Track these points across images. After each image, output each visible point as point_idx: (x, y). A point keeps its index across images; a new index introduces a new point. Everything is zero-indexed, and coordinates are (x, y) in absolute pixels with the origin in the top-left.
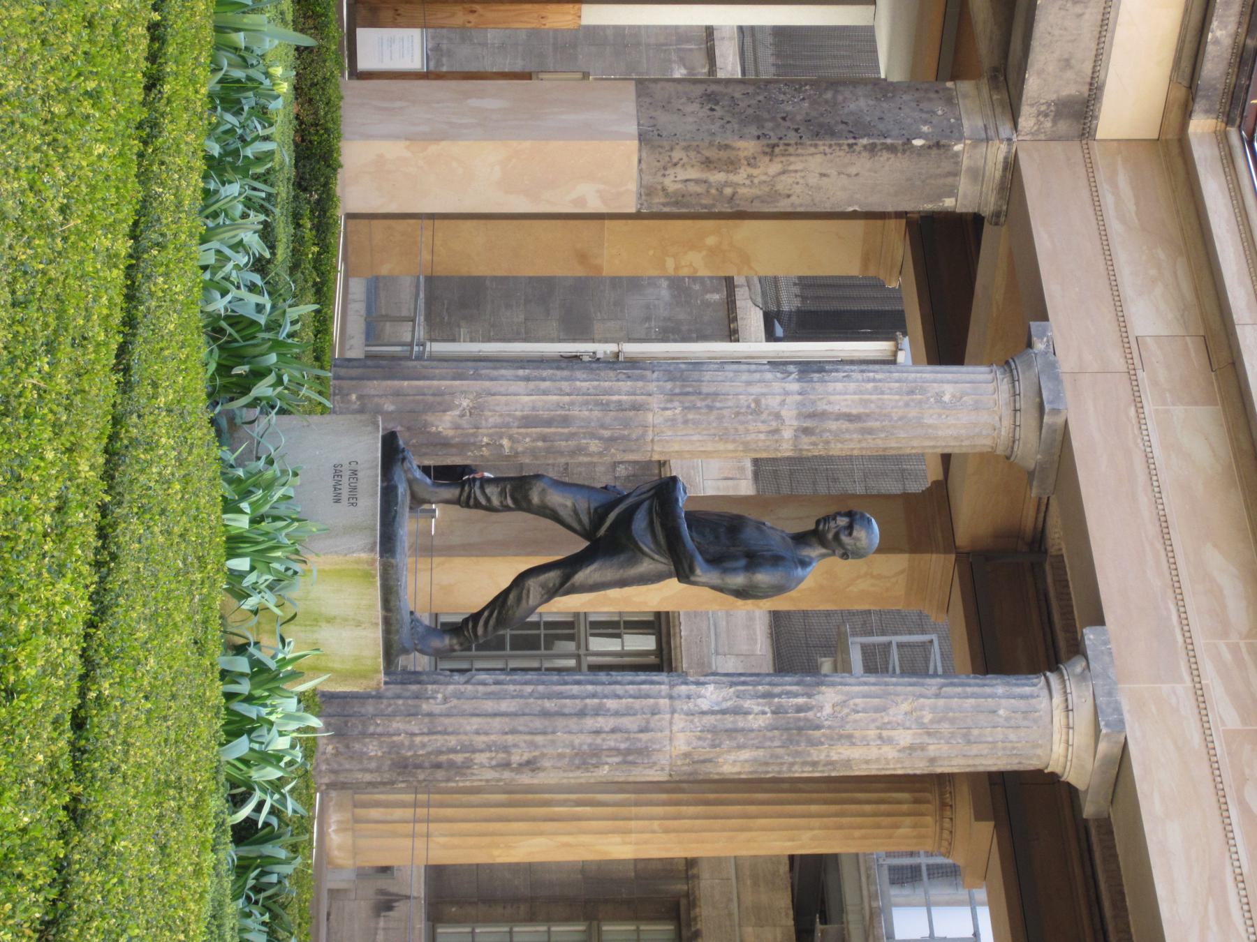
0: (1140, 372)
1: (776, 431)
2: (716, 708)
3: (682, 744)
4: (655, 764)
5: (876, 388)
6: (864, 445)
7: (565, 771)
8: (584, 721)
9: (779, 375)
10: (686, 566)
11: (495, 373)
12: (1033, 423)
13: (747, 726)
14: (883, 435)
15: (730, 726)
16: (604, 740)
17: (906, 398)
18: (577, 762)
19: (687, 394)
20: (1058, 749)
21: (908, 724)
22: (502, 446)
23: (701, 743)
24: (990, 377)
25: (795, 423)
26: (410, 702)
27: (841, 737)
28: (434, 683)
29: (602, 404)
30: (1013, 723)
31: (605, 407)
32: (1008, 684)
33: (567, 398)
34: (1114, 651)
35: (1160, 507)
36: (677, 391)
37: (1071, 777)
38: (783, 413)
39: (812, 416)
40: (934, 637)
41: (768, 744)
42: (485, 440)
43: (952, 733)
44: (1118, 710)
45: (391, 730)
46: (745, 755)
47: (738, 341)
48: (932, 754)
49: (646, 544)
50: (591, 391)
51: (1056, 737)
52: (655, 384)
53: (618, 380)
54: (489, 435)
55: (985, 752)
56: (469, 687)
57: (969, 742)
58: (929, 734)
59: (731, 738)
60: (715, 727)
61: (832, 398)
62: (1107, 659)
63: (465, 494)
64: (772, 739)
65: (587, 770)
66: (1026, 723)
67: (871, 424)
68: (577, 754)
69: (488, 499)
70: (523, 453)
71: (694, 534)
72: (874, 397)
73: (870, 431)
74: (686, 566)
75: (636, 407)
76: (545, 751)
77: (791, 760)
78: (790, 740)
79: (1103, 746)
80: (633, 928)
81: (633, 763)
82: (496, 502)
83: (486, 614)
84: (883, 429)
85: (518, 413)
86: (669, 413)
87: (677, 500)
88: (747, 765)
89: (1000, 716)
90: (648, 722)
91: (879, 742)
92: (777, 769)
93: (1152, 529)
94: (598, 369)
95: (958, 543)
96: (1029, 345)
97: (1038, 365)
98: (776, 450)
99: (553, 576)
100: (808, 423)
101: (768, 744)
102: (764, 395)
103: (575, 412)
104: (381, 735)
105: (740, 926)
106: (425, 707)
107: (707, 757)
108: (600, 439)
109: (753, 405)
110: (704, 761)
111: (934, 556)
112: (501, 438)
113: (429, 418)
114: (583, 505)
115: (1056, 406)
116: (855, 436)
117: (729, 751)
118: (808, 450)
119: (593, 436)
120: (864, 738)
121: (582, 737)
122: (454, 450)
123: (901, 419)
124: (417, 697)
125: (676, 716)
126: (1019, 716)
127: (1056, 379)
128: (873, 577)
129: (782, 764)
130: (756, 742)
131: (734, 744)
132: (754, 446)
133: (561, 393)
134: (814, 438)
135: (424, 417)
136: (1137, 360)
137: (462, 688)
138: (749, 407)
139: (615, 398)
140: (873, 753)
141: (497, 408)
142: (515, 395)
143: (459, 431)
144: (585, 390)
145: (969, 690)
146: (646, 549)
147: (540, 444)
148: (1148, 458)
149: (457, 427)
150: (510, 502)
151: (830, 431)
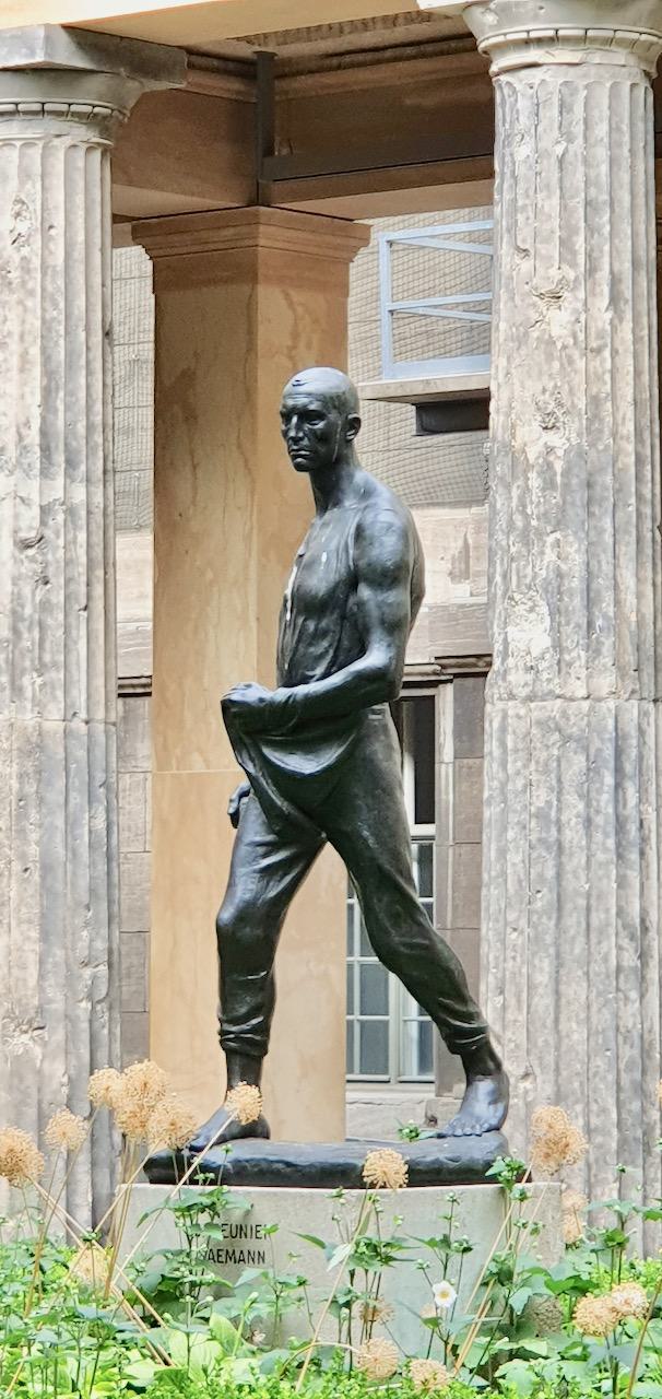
115: (40, 42)
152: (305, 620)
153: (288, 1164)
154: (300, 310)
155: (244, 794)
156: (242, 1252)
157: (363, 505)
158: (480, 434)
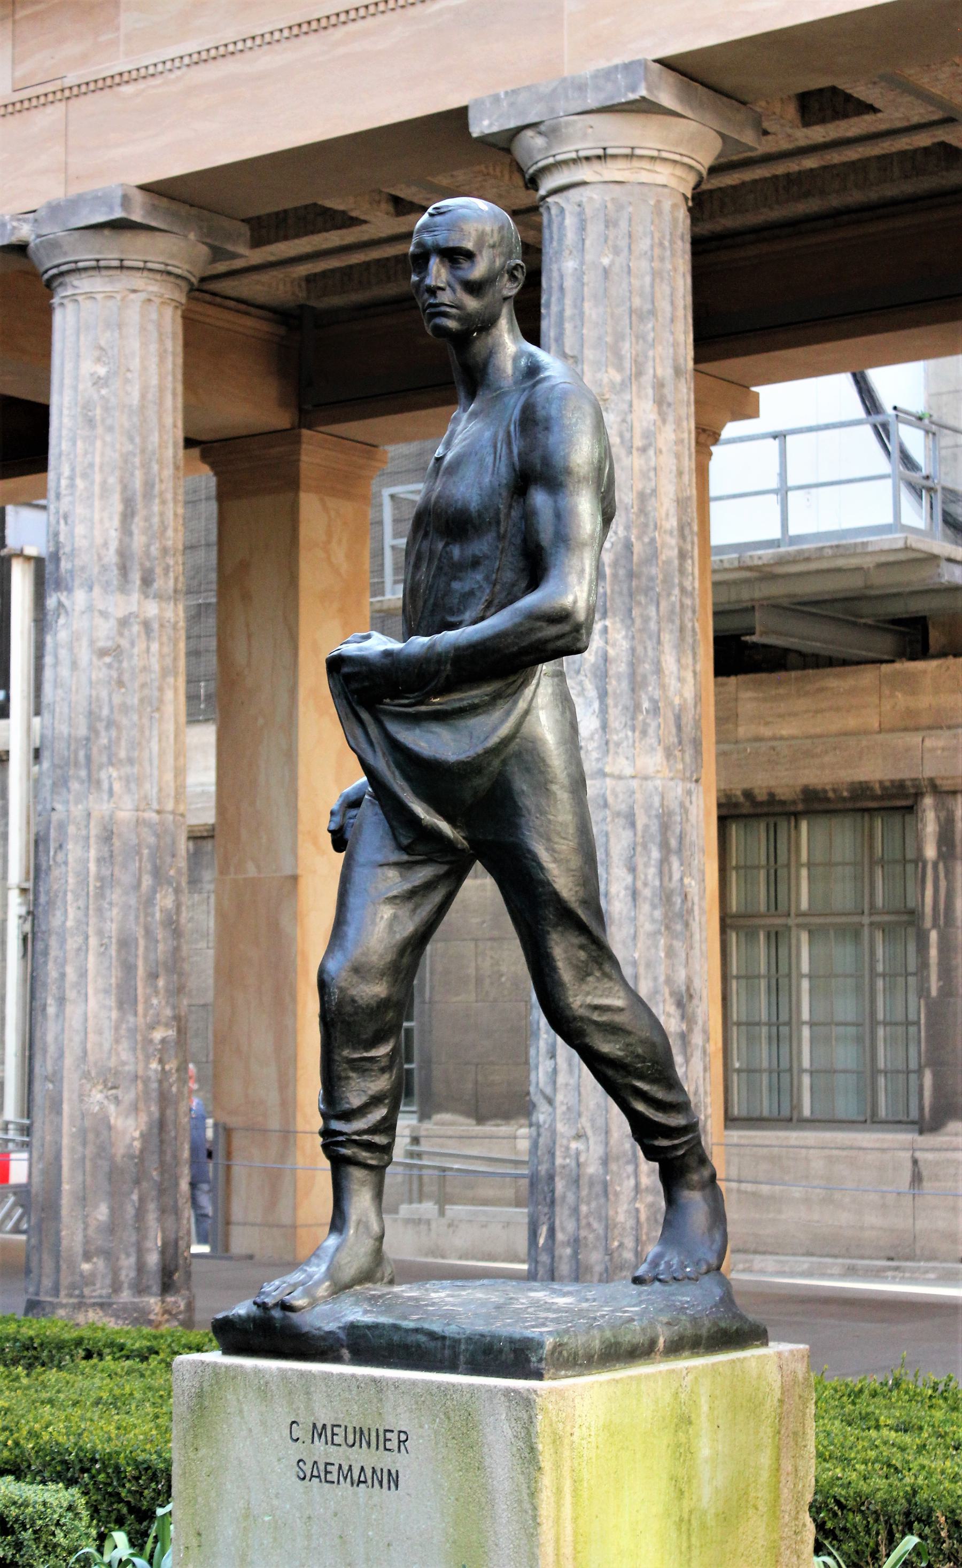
0: (68, 82)
1: (146, 625)
2: (596, 705)
3: (653, 762)
4: (682, 805)
5: (84, 476)
6: (169, 496)
7: (692, 948)
8: (616, 916)
9: (62, 621)
10: (552, 631)
11: (52, 1049)
12: (142, 240)
13: (625, 657)
14: (155, 467)
15: (625, 685)
16: (645, 884)
17: (100, 430)
18: (679, 927)
19: (88, 758)
20: (663, 175)
21: (625, 407)
22: (163, 1041)
23: (651, 731)
24: (70, 306)
25: (136, 596)
26: (584, 1193)
27: (642, 511)
28: (552, 1154)
29: (101, 888)
30: (623, 243)
31: (105, 883)
32: (559, 253)
33: (93, 941)
34: (509, 88)
35: (277, 35)
36: (83, 773)
37: (705, 159)
38: (120, 614)
39: (124, 570)
40: (386, 492)
41: (653, 625)
42: (154, 1065)
43: (637, 337)
44: (608, 74)
45: (631, 1223)
46: (669, 662)
47: (7, 752)
48: (670, 371)
49: (490, 728)
50: (81, 903)
51: (644, 177)
52: (72, 808)
53: (66, 863)
54: (147, 1059)
55: (667, 290)
56: (560, 1097)
57: (653, 312)
58: (639, 374)
59: (645, 684)
60: (626, 708)
61: (99, 540)
62: (522, 98)
63: (364, 1155)
64: (646, 619)
65: (690, 911)
66: (623, 225)
67: (138, 483)
68: (668, 927)
69: (375, 1101)
70: (174, 1008)
71: (467, 616)
72: (98, 478)
73: (148, 485)
74: (552, 631)
75: (108, 836)
76: (662, 978)
77: (676, 591)
78: (647, 591)
79: (666, 99)
80: (734, 874)
81: (681, 838)
82: (381, 1084)
83: (640, 1107)
84: (145, 466)
85: (114, 1014)
86: (117, 787)
87: (387, 654)
88: (683, 661)
89: (612, 263)
90: (618, 814)
91: (651, 452)
92: (689, 614)
93: (312, 45)
94: (48, 893)
95: (288, 426)
96: (21, 249)
97: (53, 230)
98: (175, 627)
99: (563, 950)
100: (136, 577)
101: (653, 625)
102: (92, 642)
103: (112, 928)
104: (637, 1240)
105: (737, 742)
106: (592, 1169)
107: (671, 722)
108: (154, 892)
109: (108, 660)
110: (679, 728)
111: (304, 458)
112: (151, 1041)
113: (120, 1151)
114: (394, 881)
115: (118, 201)
116: (156, 509)
117: (663, 687)
118: (176, 579)
119: (149, 902)
120: (645, 475)
121: (641, 918)
122: (169, 1112)
123: (131, 440)
124: (576, 1181)
125: (608, 769)
126: (612, 233)
127: (74, 204)
128: (329, 541)
129: (682, 606)
130: (650, 645)
131: (653, 679)
132: (169, 661)
133: (83, 949)
134: (158, 570)
135: (118, 1159)
136: (49, 88)
137: (561, 1109)
138: (109, 666)
139: (92, 867)
140: (668, 462)
141: (106, 1046)
142: (86, 1020)
143: (141, 1105)
144: (81, 914)
145: (568, 312)
146: (504, 731)
147: (161, 983)
148: (200, 59)
149: (135, 1108)
150: (382, 1051)
151: (148, 546)
152: (447, 544)
153: (432, 1335)
154: (333, 514)
155: (353, 803)
156: (362, 1469)
157: (530, 383)
158: (798, 121)
